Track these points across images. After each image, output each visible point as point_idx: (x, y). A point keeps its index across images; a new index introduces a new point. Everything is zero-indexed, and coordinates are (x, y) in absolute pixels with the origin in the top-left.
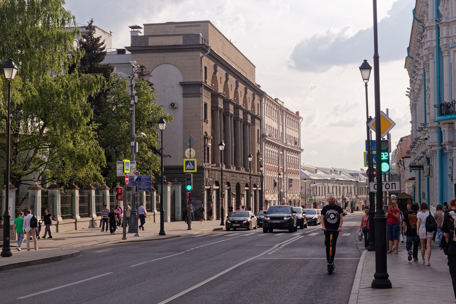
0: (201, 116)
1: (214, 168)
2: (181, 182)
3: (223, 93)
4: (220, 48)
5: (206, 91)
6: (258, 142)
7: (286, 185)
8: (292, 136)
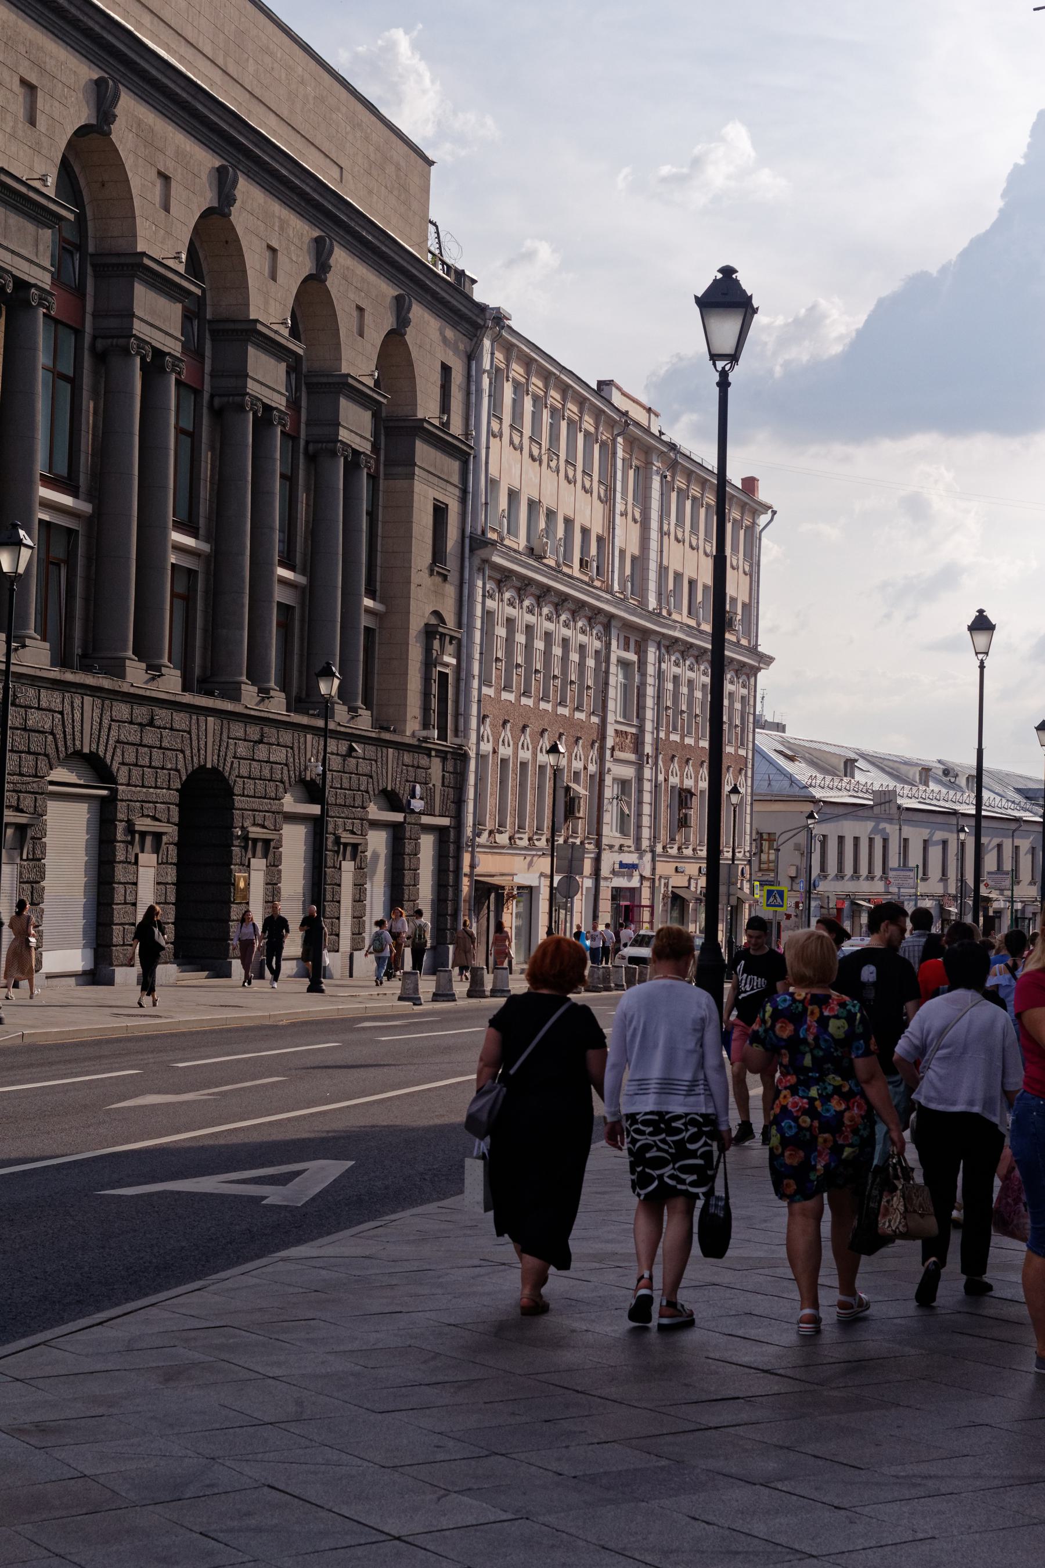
3: (436, 422)
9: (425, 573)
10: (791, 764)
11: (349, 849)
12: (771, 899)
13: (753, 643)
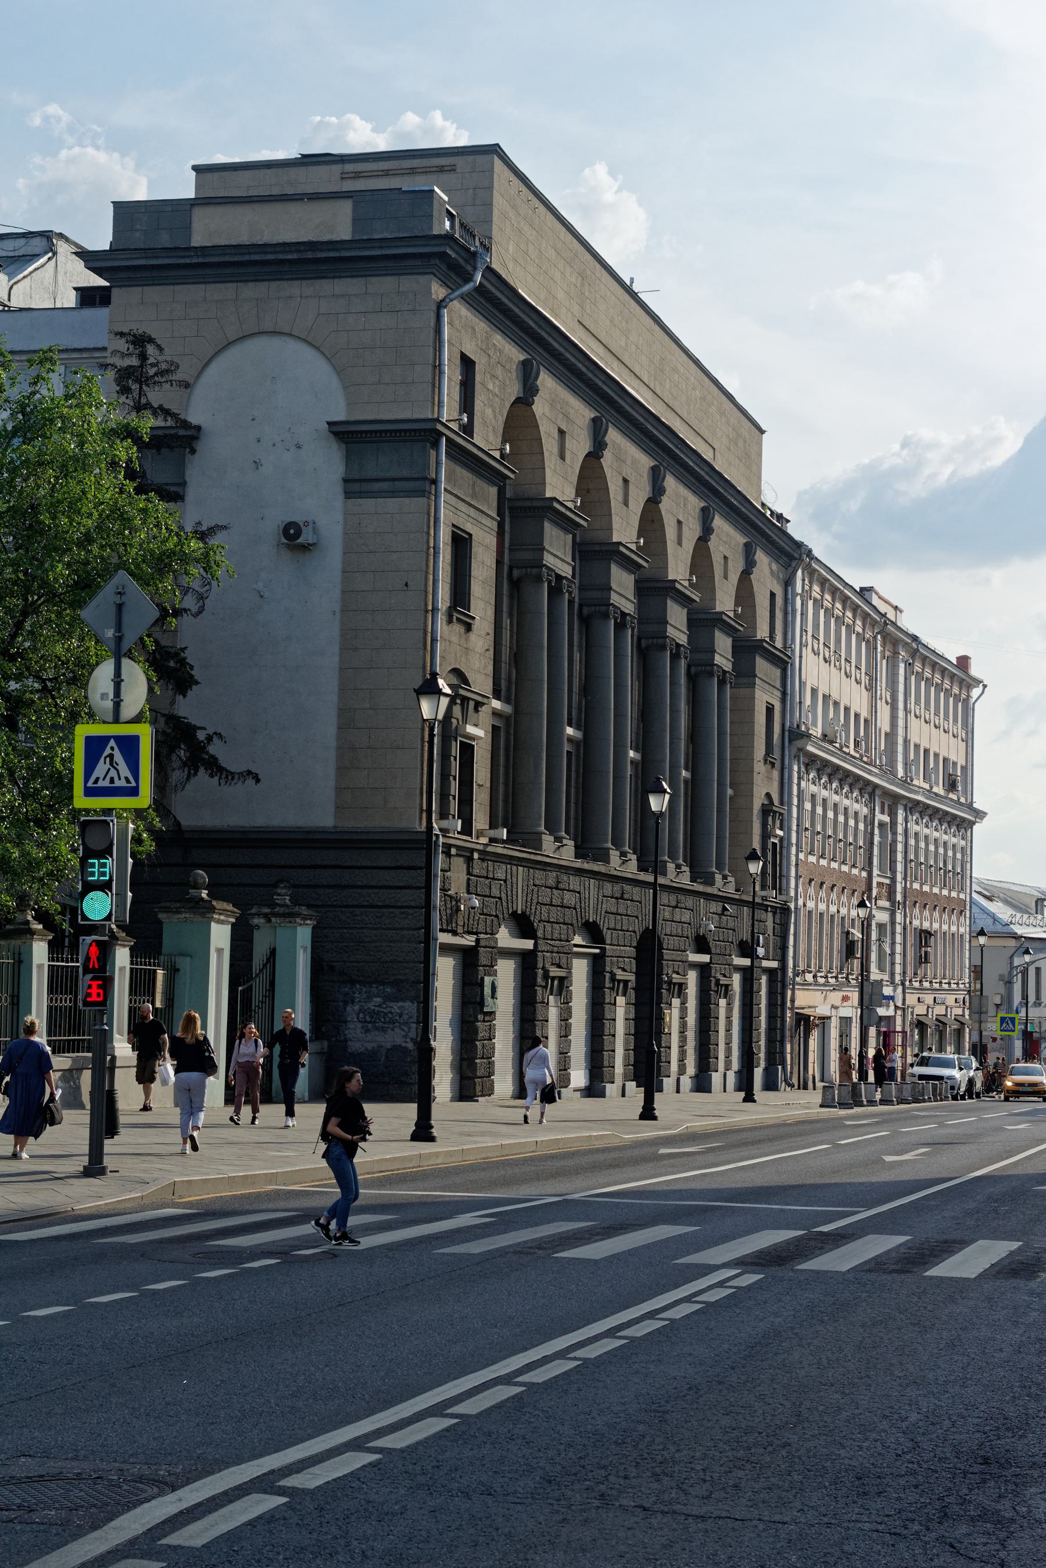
0: (430, 589)
1: (500, 851)
2: (309, 906)
4: (561, 295)
5: (464, 474)
6: (765, 761)
7: (904, 956)
8: (936, 755)
9: (762, 764)
10: (990, 903)
11: (621, 985)
12: (1004, 1025)
13: (969, 800)
